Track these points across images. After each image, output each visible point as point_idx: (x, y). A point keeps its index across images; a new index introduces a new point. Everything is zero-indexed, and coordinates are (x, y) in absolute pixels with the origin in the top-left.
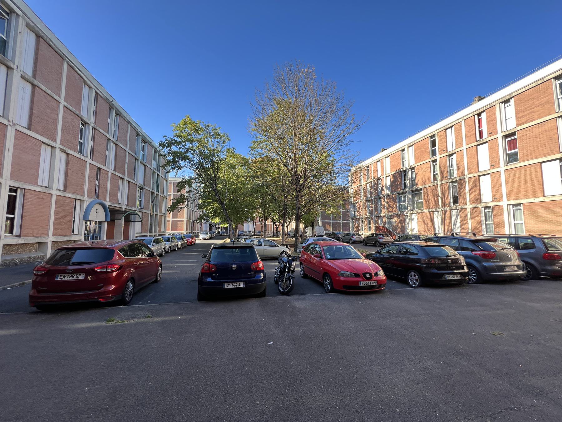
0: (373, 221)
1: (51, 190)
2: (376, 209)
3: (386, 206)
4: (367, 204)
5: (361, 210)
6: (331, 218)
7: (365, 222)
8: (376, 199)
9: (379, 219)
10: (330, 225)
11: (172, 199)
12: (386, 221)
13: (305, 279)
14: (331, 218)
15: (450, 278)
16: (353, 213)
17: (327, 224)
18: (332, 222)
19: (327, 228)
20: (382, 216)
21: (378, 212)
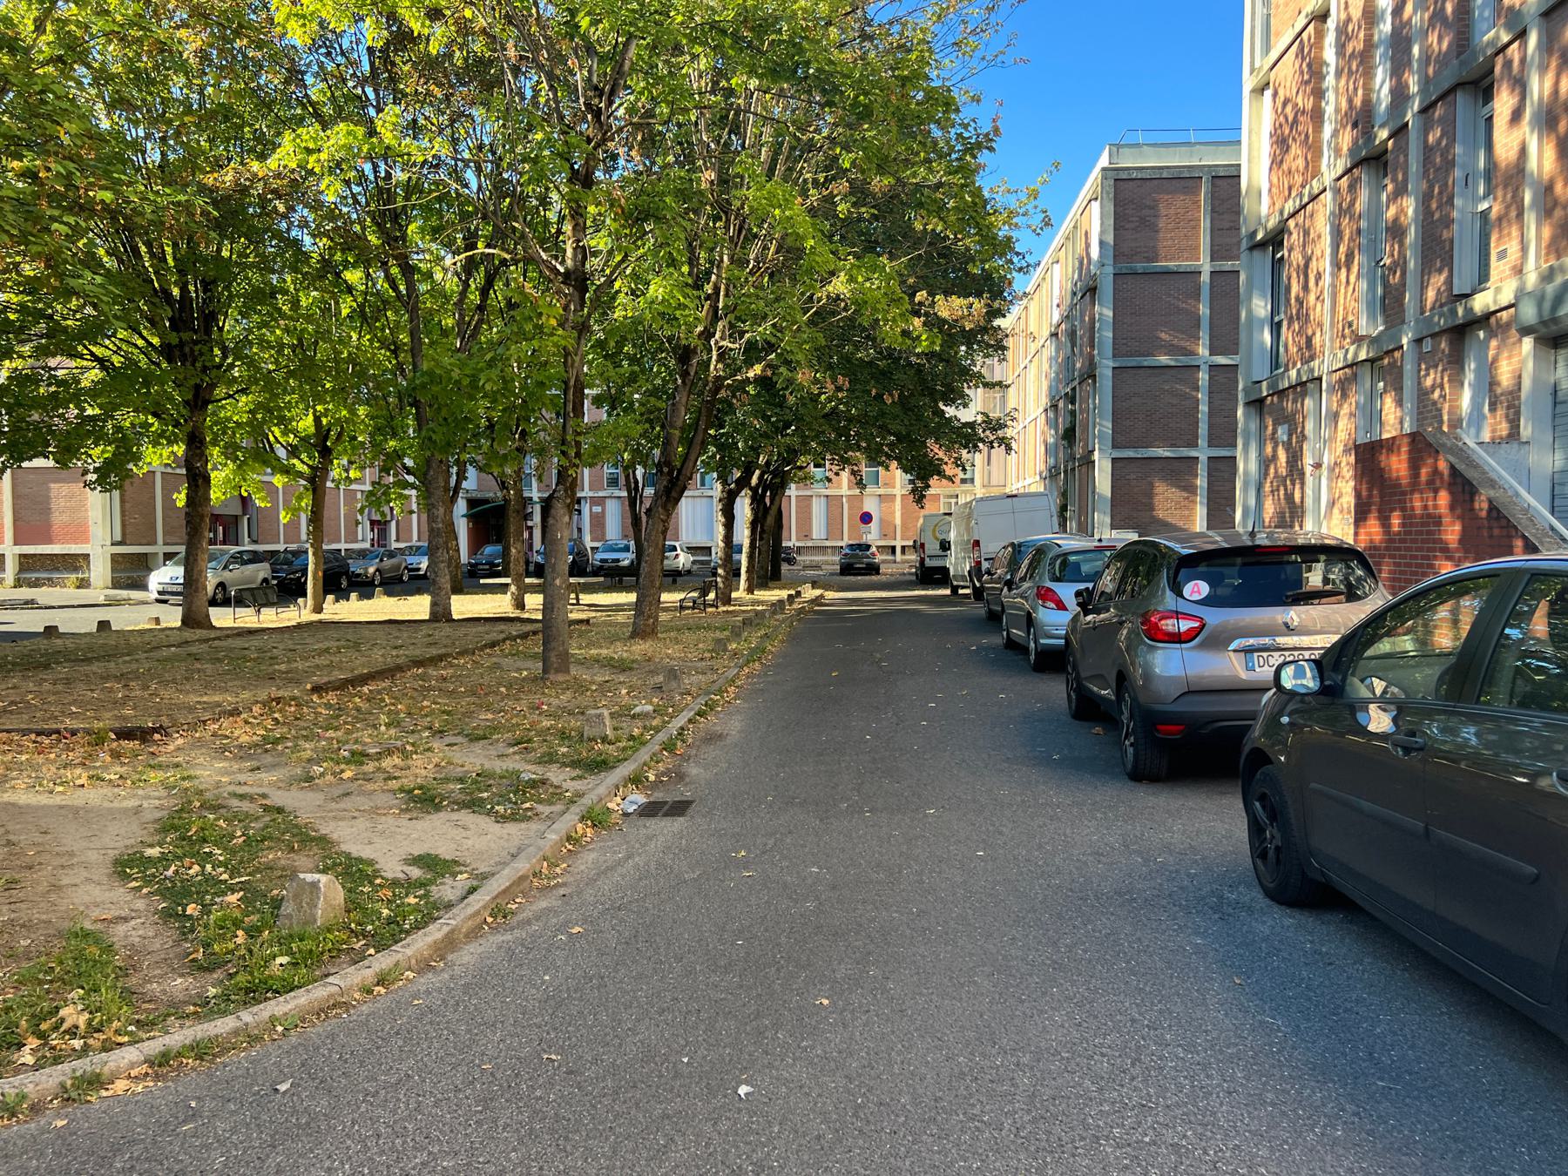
0: (1399, 402)
1: (1265, 297)
2: (1436, 250)
3: (1532, 164)
4: (1361, 205)
5: (1312, 297)
6: (1203, 429)
7: (1335, 417)
8: (1439, 112)
9: (1456, 362)
10: (1191, 489)
11: (413, 512)
12: (1527, 383)
13: (1307, 920)
14: (1203, 429)
15: (228, 623)
16: (1262, 343)
17: (1164, 479)
18: (1203, 458)
19: (1160, 514)
20: (1488, 316)
21: (1449, 282)
